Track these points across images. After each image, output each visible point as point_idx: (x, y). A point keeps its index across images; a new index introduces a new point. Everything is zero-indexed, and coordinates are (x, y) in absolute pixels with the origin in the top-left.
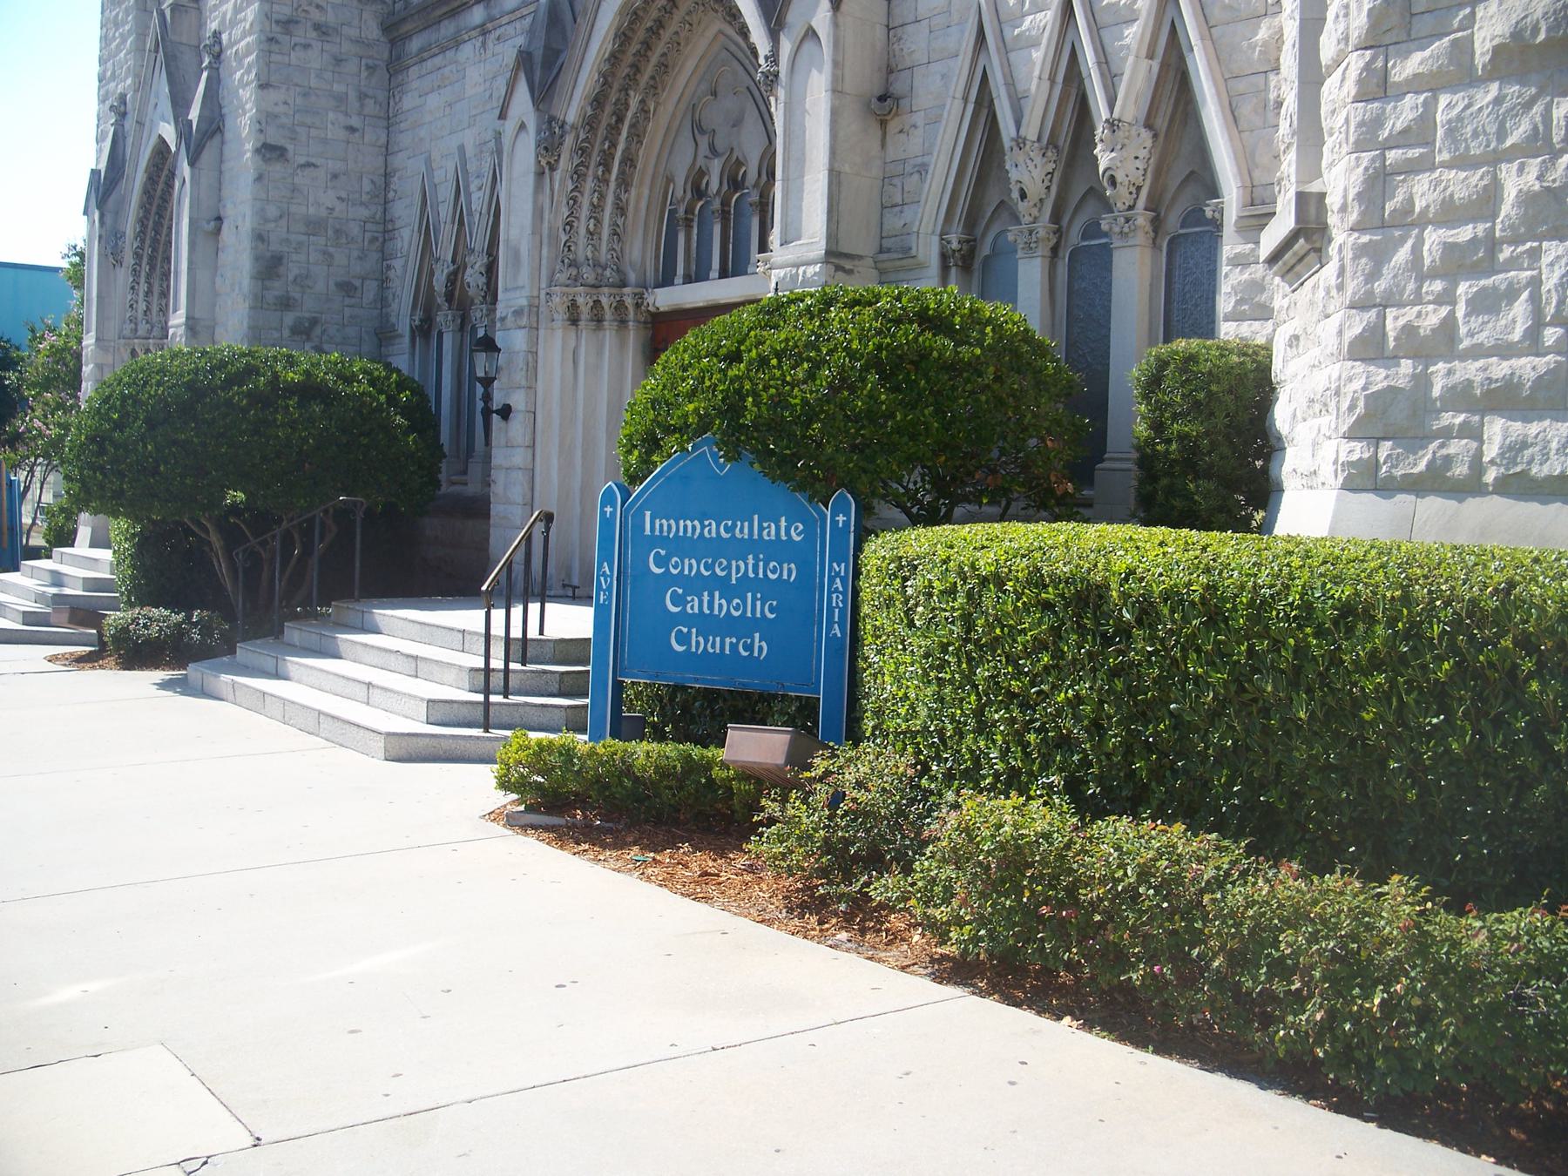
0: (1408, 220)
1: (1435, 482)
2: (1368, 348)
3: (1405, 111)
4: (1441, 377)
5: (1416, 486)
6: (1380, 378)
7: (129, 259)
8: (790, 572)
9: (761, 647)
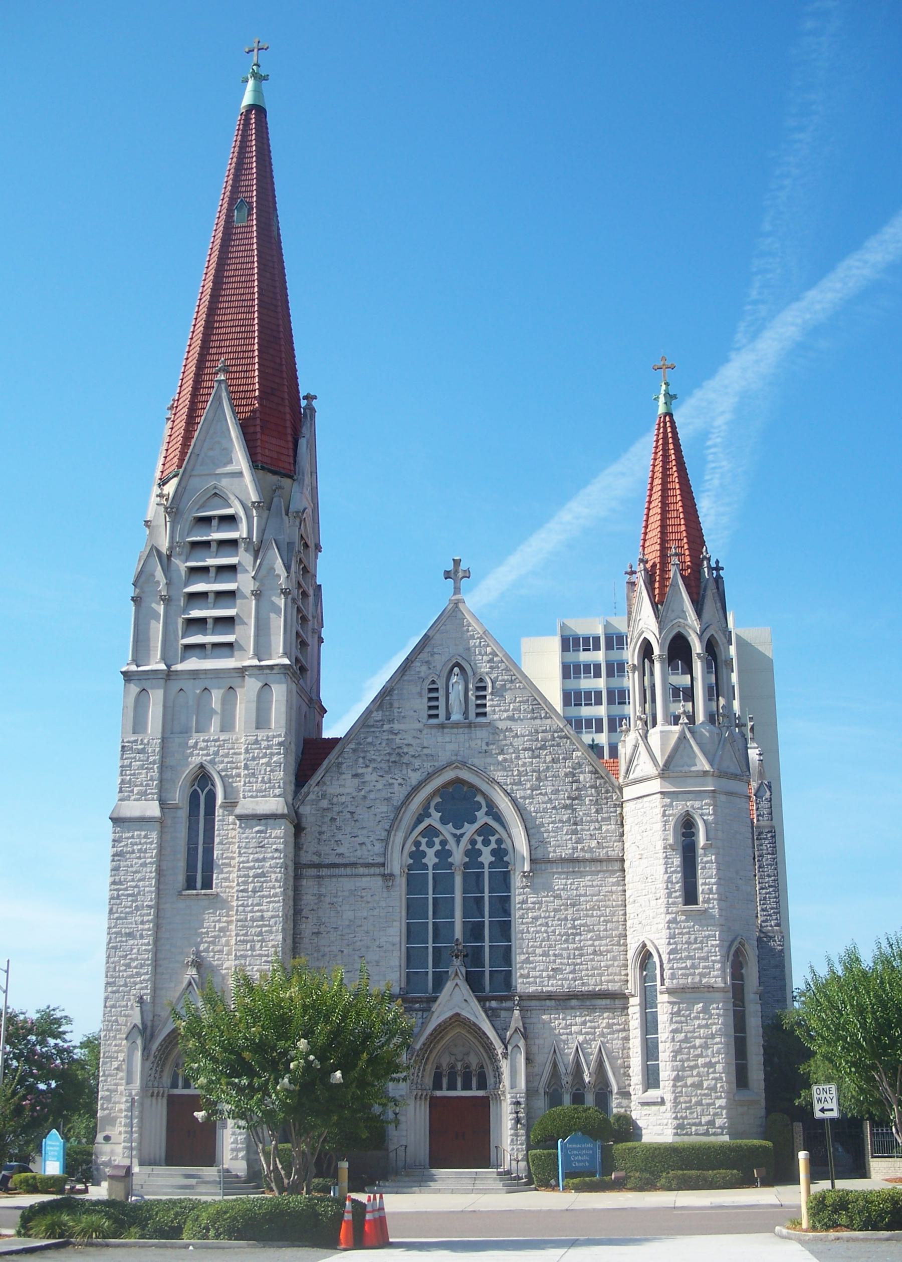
0: (680, 1103)
1: (686, 1134)
2: (676, 1118)
3: (679, 1089)
5: (684, 1135)
6: (678, 1122)
7: (152, 1058)
8: (591, 1152)
9: (587, 1164)
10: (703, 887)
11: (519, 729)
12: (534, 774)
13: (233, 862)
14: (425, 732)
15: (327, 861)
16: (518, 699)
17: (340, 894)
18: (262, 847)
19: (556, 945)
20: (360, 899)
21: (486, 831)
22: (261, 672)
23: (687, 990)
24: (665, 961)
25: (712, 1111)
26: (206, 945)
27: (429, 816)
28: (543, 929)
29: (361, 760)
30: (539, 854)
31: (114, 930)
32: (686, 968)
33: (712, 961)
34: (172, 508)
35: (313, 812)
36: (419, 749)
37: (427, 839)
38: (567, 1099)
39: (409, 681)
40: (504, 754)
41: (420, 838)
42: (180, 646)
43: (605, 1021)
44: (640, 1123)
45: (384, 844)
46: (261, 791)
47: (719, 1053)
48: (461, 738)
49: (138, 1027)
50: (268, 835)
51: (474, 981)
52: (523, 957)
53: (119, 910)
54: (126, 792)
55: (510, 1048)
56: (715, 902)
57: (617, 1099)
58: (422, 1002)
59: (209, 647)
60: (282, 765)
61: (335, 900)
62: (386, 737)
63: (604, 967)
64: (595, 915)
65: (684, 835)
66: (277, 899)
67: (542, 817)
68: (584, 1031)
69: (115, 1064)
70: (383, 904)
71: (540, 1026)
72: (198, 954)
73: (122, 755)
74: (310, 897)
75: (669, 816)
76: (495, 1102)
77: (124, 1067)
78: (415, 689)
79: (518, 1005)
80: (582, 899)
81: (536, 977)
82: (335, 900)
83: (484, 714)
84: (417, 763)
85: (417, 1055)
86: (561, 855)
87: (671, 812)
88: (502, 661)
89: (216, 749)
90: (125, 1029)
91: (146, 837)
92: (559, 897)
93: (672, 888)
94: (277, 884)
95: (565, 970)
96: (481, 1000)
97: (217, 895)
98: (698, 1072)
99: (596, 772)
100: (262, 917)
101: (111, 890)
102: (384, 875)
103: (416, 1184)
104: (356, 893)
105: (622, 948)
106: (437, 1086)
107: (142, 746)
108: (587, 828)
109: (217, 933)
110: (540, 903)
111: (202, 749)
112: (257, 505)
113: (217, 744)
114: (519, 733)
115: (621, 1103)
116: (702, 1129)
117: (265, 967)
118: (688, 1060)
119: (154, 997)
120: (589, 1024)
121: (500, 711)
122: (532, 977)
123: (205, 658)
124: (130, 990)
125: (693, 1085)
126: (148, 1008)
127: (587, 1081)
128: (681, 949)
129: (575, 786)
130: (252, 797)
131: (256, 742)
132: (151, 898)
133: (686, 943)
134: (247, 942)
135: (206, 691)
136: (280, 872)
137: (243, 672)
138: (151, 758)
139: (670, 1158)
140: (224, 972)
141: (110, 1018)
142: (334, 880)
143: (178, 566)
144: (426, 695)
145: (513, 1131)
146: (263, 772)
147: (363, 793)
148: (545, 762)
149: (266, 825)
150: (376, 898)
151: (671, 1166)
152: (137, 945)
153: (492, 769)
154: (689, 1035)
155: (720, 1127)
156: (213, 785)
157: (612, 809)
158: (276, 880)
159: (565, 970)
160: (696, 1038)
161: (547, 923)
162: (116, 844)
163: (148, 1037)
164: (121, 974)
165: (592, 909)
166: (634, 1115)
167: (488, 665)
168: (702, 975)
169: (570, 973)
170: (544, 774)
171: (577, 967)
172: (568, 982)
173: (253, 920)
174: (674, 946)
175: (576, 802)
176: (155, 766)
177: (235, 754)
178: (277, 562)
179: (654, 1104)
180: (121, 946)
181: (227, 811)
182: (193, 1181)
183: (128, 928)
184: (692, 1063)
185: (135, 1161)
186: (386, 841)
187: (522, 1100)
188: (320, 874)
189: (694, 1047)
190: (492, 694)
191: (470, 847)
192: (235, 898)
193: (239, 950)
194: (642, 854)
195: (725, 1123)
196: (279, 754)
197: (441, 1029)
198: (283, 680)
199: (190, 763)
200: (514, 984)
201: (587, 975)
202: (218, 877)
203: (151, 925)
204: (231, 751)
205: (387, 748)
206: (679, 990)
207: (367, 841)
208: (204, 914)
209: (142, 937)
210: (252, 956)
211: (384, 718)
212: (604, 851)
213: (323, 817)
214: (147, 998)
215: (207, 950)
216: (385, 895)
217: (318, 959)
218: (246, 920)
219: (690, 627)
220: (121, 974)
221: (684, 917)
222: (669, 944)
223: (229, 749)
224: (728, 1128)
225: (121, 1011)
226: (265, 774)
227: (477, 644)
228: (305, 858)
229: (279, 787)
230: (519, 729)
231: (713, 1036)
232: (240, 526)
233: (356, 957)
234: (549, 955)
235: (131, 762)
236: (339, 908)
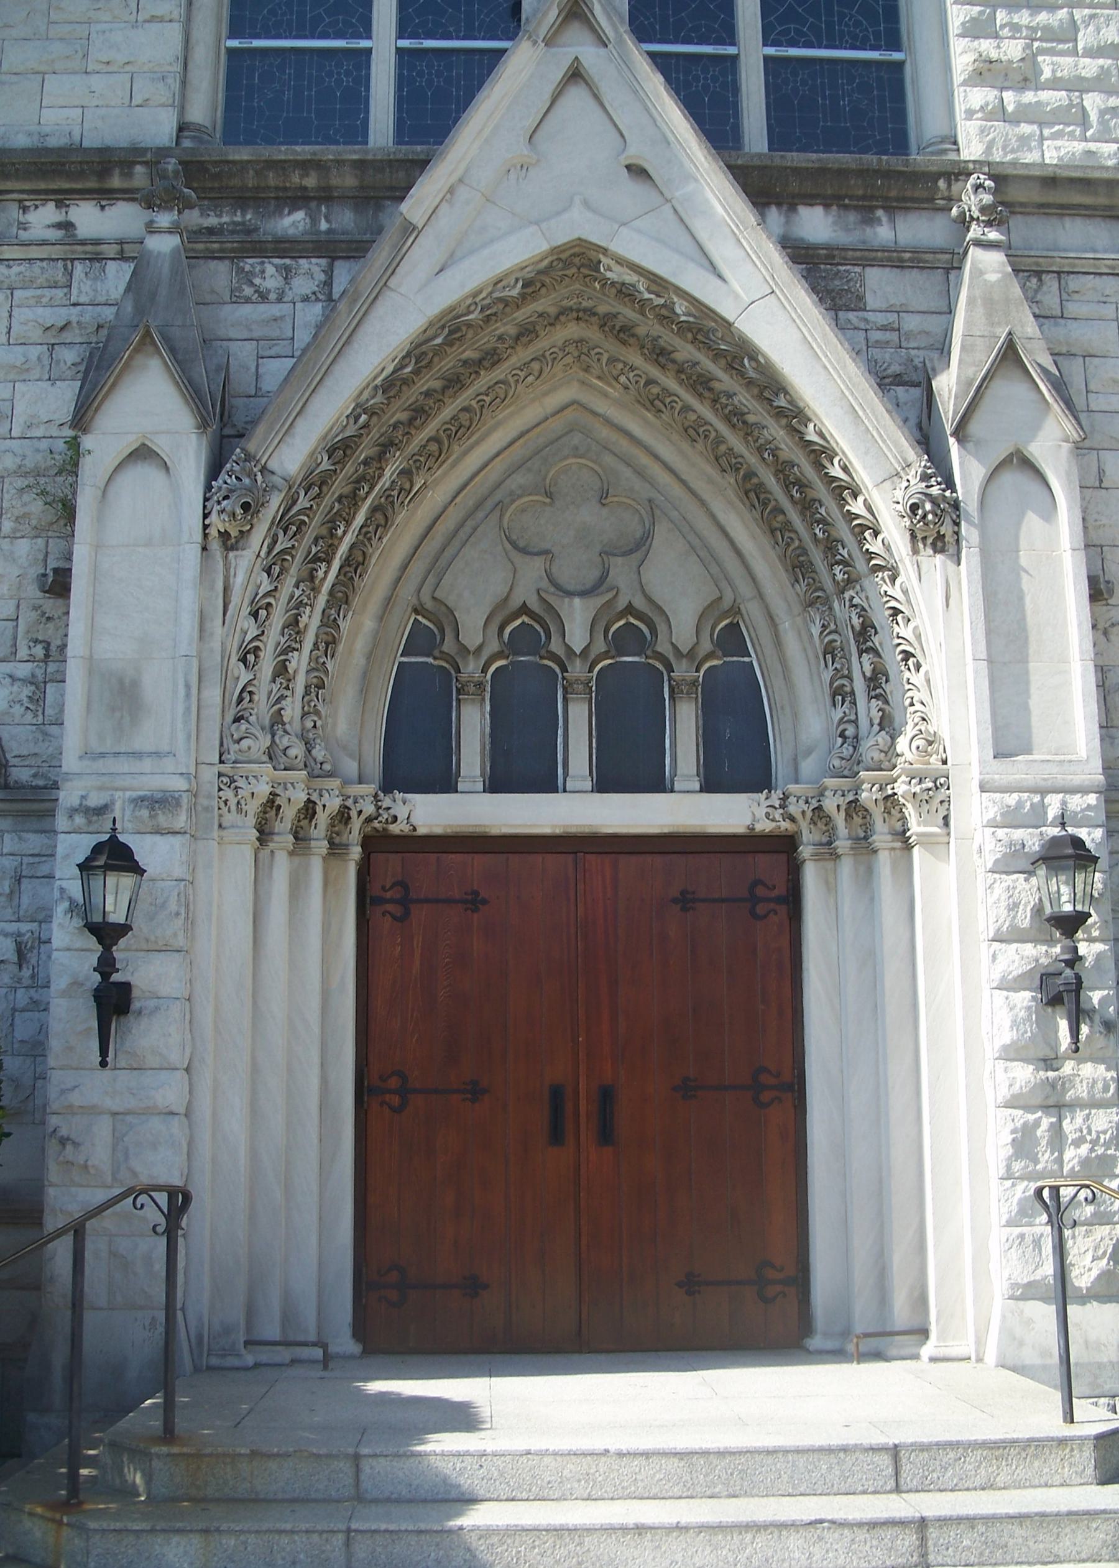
58: (326, 196)
81: (1078, 85)
85: (285, 523)
122: (1055, 84)
145: (1024, 1074)
187: (1092, 837)
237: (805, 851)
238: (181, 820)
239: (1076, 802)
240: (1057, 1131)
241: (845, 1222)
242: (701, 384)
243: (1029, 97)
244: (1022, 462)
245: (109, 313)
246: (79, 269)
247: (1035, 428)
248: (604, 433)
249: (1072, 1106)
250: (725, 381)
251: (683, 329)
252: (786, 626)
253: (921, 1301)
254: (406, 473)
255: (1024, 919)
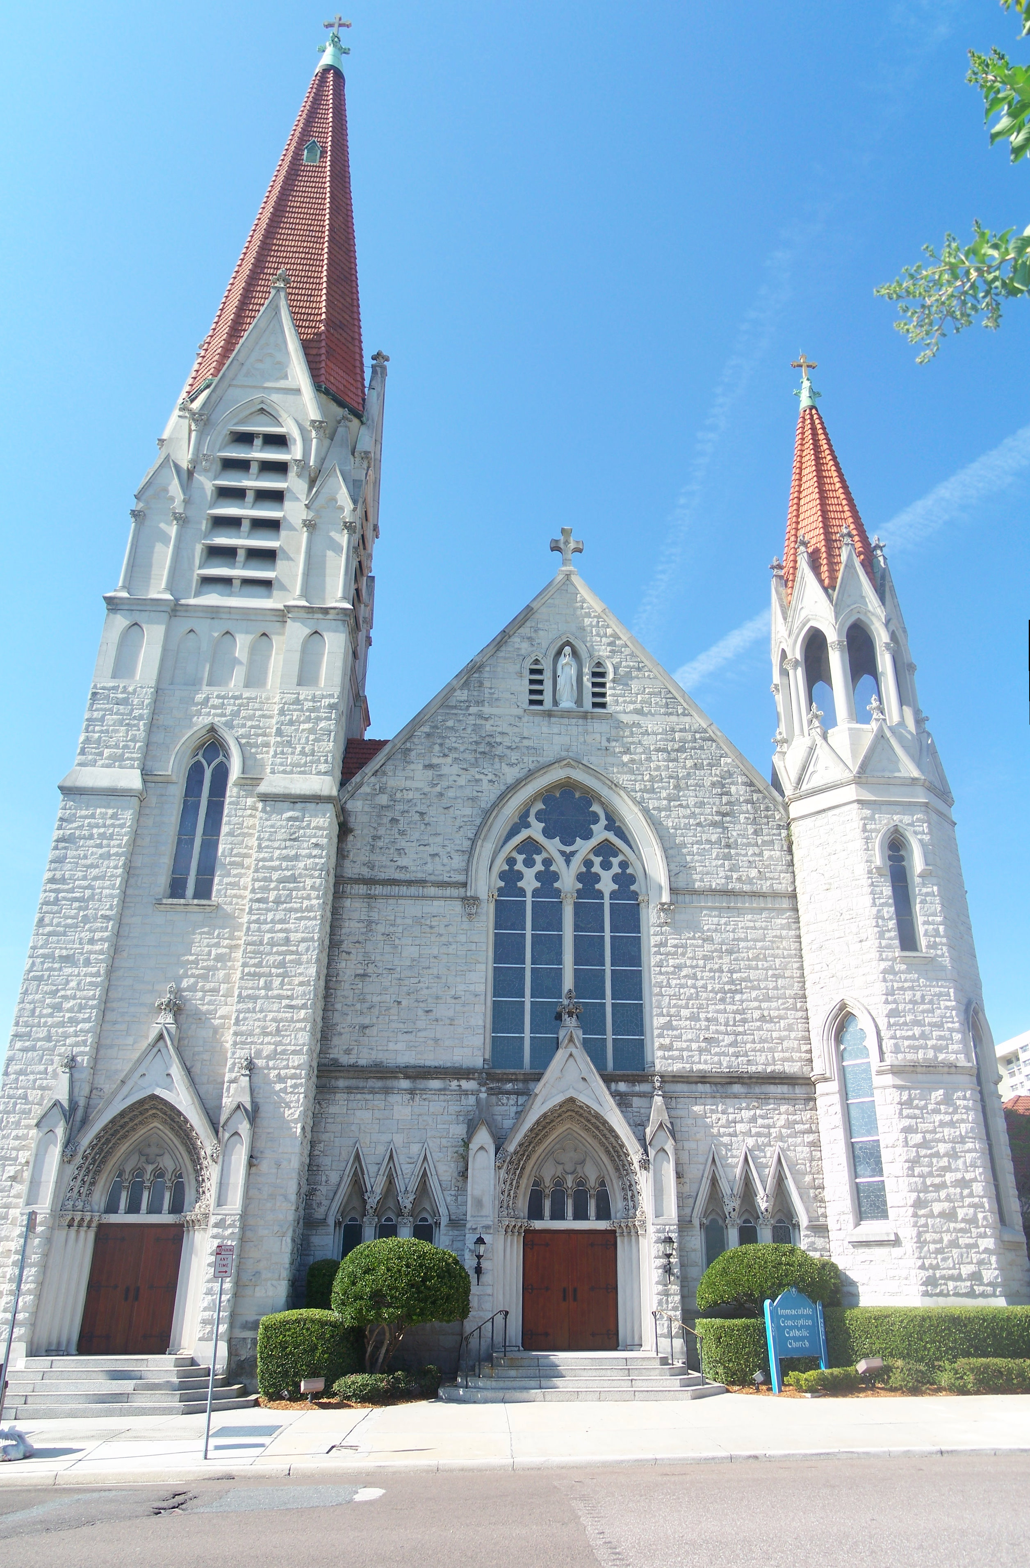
1: (941, 1294)
2: (922, 1267)
3: (922, 1221)
4: (938, 1274)
5: (937, 1295)
7: (78, 1160)
8: (810, 1323)
10: (926, 927)
11: (649, 726)
12: (672, 781)
13: (247, 861)
14: (525, 719)
15: (383, 876)
16: (647, 690)
17: (399, 921)
18: (295, 840)
19: (708, 1005)
20: (428, 930)
21: (606, 850)
22: (310, 616)
23: (919, 1069)
24: (883, 1026)
25: (975, 1258)
26: (192, 980)
27: (528, 826)
28: (690, 982)
29: (437, 748)
30: (681, 883)
31: (41, 951)
32: (913, 1038)
33: (949, 1029)
34: (201, 415)
35: (366, 809)
36: (517, 740)
37: (524, 856)
38: (765, 1234)
39: (505, 658)
40: (631, 754)
41: (514, 854)
42: (195, 577)
43: (784, 1117)
44: (853, 1275)
45: (466, 857)
46: (298, 765)
47: (974, 1165)
48: (574, 730)
49: (62, 1106)
50: (305, 824)
51: (595, 1052)
52: (663, 1020)
53: (55, 921)
54: (91, 754)
55: (652, 1152)
56: (945, 948)
57: (806, 1236)
58: (516, 1080)
59: (237, 583)
60: (333, 734)
61: (392, 929)
62: (474, 722)
63: (776, 1038)
64: (760, 966)
65: (890, 858)
66: (312, 914)
67: (682, 835)
68: (754, 1130)
69: (11, 1171)
70: (463, 938)
71: (690, 1121)
72: (177, 992)
73: (92, 705)
74: (354, 924)
75: (871, 831)
76: (626, 1239)
77: (26, 1175)
78: (513, 668)
79: (660, 1088)
80: (742, 944)
81: (682, 1050)
82: (392, 929)
83: (603, 705)
84: (514, 756)
85: (510, 1162)
86: (711, 885)
87: (873, 826)
88: (626, 646)
89: (236, 708)
90: (38, 1111)
91: (114, 816)
92: (709, 940)
93: (884, 926)
94: (314, 894)
95: (723, 1041)
96: (608, 1079)
97: (218, 907)
98: (948, 1195)
99: (751, 784)
100: (287, 941)
101: (45, 891)
102: (464, 899)
103: (533, 1383)
104: (423, 921)
105: (800, 1014)
106: (535, 1213)
107: (125, 695)
108: (743, 852)
109: (212, 963)
110: (684, 946)
111: (214, 707)
112: (318, 425)
113: (237, 702)
114: (650, 730)
115: (814, 1243)
116: (964, 1287)
117: (284, 1015)
118: (930, 1174)
119: (95, 1059)
120: (760, 1121)
121: (625, 702)
122: (677, 1050)
123: (230, 595)
124: (55, 1046)
125: (942, 1215)
126: (83, 1076)
127: (763, 1208)
128: (904, 1011)
129: (725, 799)
130: (284, 772)
131: (297, 701)
132: (111, 905)
133: (911, 1002)
134: (260, 975)
135: (228, 636)
136: (320, 877)
137: (284, 616)
138: (135, 711)
139: (950, 1335)
140: (216, 1022)
141: (11, 1091)
142: (391, 901)
143: (202, 484)
144: (528, 676)
145: (660, 1287)
146: (303, 741)
147: (438, 789)
148: (684, 767)
149: (303, 810)
150: (452, 929)
151: (951, 1348)
152: (79, 975)
153: (615, 770)
154: (928, 1136)
155: (990, 1284)
156: (227, 756)
157: (775, 831)
158: (313, 888)
159: (723, 1041)
160: (938, 1141)
161: (695, 974)
162: (65, 824)
163: (77, 1124)
164: (43, 1020)
165: (756, 958)
166: (834, 1260)
167: (609, 648)
168: (937, 1049)
169: (730, 1045)
170: (684, 781)
171: (739, 1038)
172: (728, 1058)
173: (272, 943)
174: (894, 1006)
175: (728, 819)
176: (141, 723)
177: (263, 716)
178: (341, 492)
179: (880, 1243)
180: (49, 976)
181: (245, 790)
182: (127, 1386)
183: (66, 948)
184: (937, 1180)
185: (20, 1348)
186: (470, 852)
187: (674, 1236)
188: (372, 892)
189: (937, 1155)
190: (614, 681)
191: (584, 870)
192: (247, 910)
193: (246, 988)
194: (830, 884)
195: (996, 1277)
196: (329, 719)
197: (546, 1123)
198: (342, 628)
199: (195, 725)
200: (649, 1058)
201: (754, 1050)
202: (221, 881)
203: (106, 945)
204: (258, 713)
205: (473, 736)
206: (907, 1068)
207: (442, 853)
208: (194, 934)
209: (87, 963)
210: (267, 997)
211: (471, 698)
212: (768, 883)
213: (379, 816)
214: (84, 1061)
215: (192, 988)
216: (465, 926)
217: (362, 1013)
218: (261, 943)
219: (873, 614)
220: (43, 1020)
221: (904, 967)
222: (887, 1002)
223: (255, 710)
224: (1002, 1285)
225: (35, 1081)
226: (307, 743)
227: (594, 623)
228: (352, 870)
229: (326, 762)
230: (649, 724)
231: (962, 1140)
232: (293, 448)
233: (420, 1012)
234: (699, 1020)
235: (104, 715)
236: (397, 942)
237: (618, 1234)
238: (492, 1231)
239: (672, 1228)
240: (667, 1300)
241: (626, 1319)
242: (597, 1128)
243: (671, 1053)
244: (663, 1150)
245: (470, 1108)
246: (463, 1097)
247: (666, 1142)
248: (576, 1135)
249: (671, 1295)
250: (602, 1127)
251: (593, 1116)
252: (614, 1181)
253: (641, 1338)
254: (534, 1147)
255: (661, 1254)
